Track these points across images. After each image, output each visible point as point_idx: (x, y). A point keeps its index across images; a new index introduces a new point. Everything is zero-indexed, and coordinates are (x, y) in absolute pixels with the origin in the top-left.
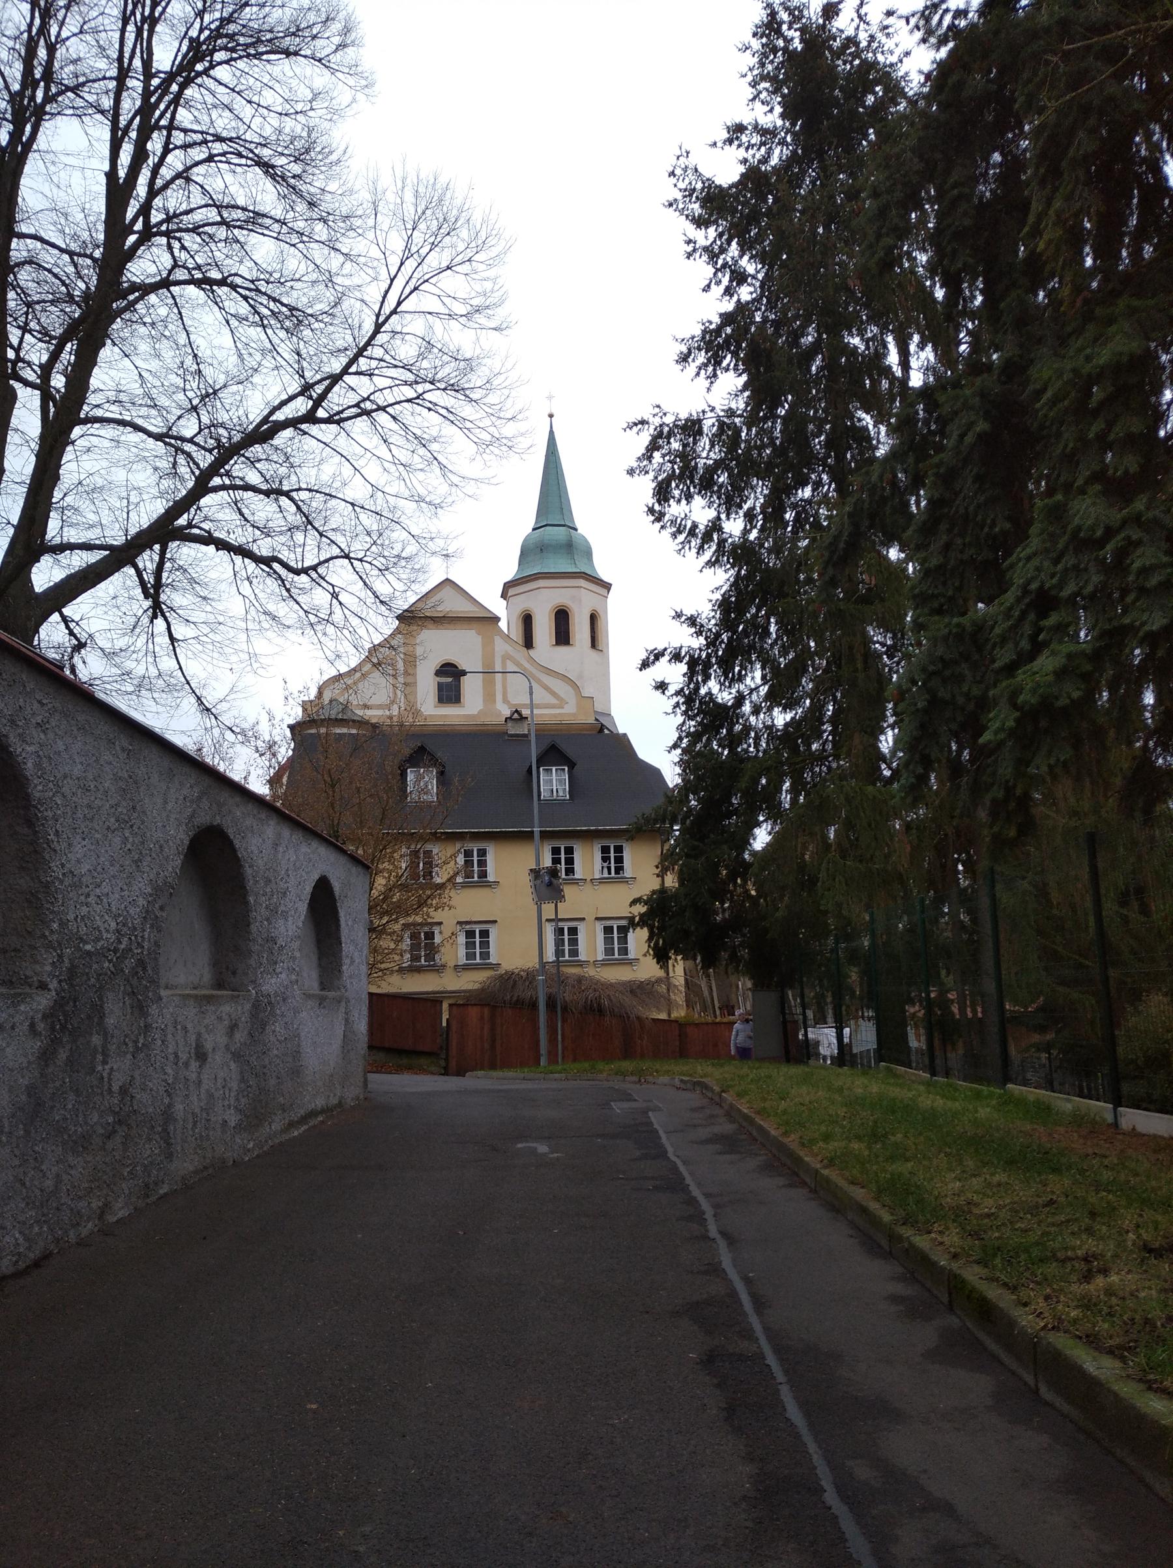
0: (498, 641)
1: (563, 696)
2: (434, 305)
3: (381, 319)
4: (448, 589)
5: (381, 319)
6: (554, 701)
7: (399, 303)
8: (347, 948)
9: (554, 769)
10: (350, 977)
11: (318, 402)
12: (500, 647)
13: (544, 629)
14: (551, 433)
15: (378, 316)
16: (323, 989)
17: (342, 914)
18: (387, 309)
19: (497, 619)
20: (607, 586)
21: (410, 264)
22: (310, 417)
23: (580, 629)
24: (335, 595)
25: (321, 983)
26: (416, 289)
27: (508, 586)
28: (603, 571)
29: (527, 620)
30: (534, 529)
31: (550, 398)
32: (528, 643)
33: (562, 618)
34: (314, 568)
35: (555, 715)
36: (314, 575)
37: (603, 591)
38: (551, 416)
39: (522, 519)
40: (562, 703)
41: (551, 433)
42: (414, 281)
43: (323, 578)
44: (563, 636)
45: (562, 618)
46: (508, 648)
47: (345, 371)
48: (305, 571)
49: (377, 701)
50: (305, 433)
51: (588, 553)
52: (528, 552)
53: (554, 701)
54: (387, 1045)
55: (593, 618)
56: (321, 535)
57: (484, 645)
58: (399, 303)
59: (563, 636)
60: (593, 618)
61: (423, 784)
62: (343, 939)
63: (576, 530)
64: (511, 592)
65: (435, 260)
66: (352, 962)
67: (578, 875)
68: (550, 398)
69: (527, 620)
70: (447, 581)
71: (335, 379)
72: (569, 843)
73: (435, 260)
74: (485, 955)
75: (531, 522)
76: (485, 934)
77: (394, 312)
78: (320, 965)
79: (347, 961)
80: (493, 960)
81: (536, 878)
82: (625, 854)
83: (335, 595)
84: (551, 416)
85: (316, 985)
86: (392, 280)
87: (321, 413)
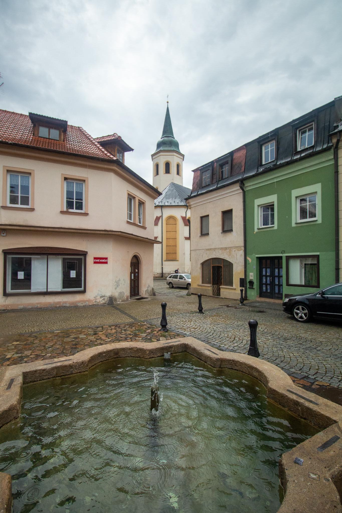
13: (162, 168)
14: (168, 108)
33: (167, 165)
39: (158, 136)
41: (168, 108)
44: (168, 171)
45: (167, 165)
52: (159, 145)
59: (168, 171)
84: (168, 102)
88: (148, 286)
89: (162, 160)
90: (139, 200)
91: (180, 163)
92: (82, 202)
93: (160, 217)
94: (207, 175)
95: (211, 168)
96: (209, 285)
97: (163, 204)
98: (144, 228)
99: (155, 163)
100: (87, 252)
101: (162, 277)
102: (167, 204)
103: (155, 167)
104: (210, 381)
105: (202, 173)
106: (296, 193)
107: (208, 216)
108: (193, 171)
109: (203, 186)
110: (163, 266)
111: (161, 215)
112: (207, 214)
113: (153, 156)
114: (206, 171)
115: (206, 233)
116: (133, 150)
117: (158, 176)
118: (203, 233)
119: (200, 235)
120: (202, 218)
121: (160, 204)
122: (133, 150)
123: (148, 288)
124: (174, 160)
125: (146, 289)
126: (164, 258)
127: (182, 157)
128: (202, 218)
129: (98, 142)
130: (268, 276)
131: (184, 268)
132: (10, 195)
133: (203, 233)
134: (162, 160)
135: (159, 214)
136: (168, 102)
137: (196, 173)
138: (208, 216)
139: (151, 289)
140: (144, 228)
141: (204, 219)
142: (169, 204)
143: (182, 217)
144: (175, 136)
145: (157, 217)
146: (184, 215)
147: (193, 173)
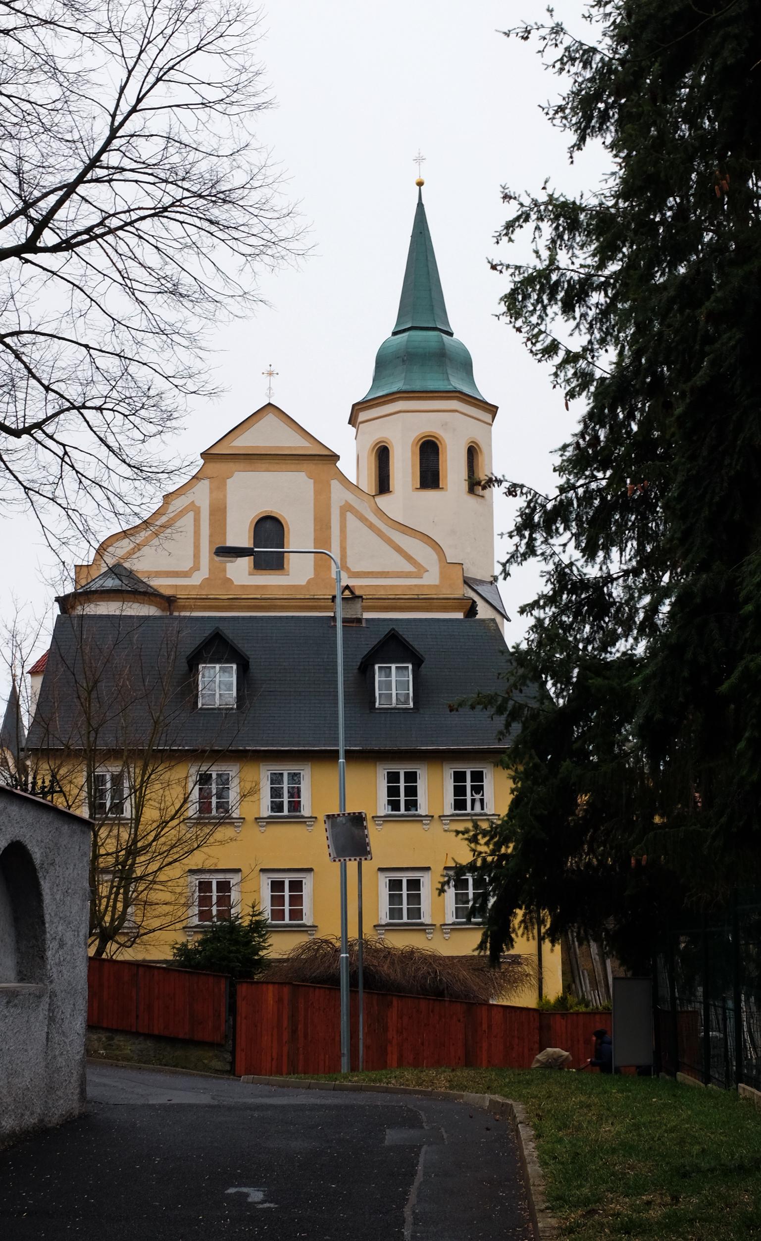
0: (335, 485)
1: (420, 560)
2: (185, 95)
3: (119, 119)
4: (270, 418)
5: (119, 119)
6: (409, 568)
7: (139, 100)
8: (53, 927)
9: (393, 666)
10: (59, 964)
11: (40, 226)
12: (338, 495)
13: (404, 467)
14: (420, 206)
15: (113, 116)
16: (21, 980)
17: (46, 886)
18: (125, 108)
19: (335, 457)
20: (493, 410)
21: (152, 50)
22: (31, 246)
23: (454, 467)
24: (64, 458)
25: (20, 973)
26: (159, 80)
27: (357, 408)
28: (486, 390)
29: (383, 454)
30: (395, 334)
31: (419, 160)
32: (383, 485)
33: (429, 451)
34: (38, 425)
35: (410, 587)
36: (39, 435)
37: (487, 417)
38: (420, 184)
39: (379, 317)
40: (421, 570)
41: (420, 206)
42: (155, 71)
43: (51, 437)
44: (430, 477)
45: (429, 451)
46: (350, 498)
47: (80, 180)
48: (27, 431)
49: (176, 564)
50: (27, 261)
51: (465, 365)
52: (385, 363)
53: (409, 568)
54: (156, 1032)
55: (472, 453)
56: (47, 389)
57: (317, 493)
58: (139, 100)
59: (430, 477)
60: (472, 453)
61: (218, 684)
62: (47, 918)
63: (451, 334)
64: (362, 416)
65: (182, 42)
66: (62, 945)
67: (422, 810)
68: (419, 160)
69: (383, 454)
70: (269, 404)
71: (70, 189)
72: (410, 768)
73: (182, 42)
74: (296, 914)
75: (391, 323)
76: (296, 886)
77: (134, 110)
78: (18, 950)
79: (54, 945)
80: (307, 920)
81: (333, 826)
82: (486, 783)
83: (64, 458)
84: (420, 184)
85: (12, 974)
86: (130, 72)
87: (48, 238)
89: (402, 430)
92: (272, 797)
100: (497, 408)
106: (410, 666)
124: (453, 429)
126: (205, 877)
129: (415, 1149)
130: (105, 871)
132: (272, 788)
134: (402, 430)
144: (454, 326)
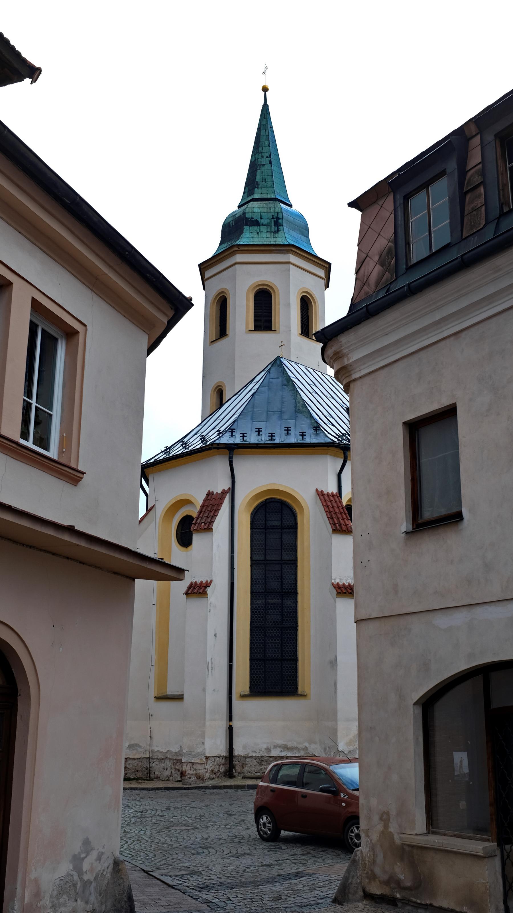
13: (241, 312)
33: (264, 303)
39: (229, 198)
59: (264, 318)
84: (265, 89)
88: (77, 847)
90: (35, 303)
91: (315, 292)
93: (224, 493)
94: (433, 214)
95: (452, 166)
96: (477, 847)
97: (238, 440)
98: (72, 475)
99: (214, 293)
101: (229, 774)
102: (253, 439)
103: (215, 310)
104: (347, 350)
105: (407, 198)
107: (449, 413)
108: (351, 205)
109: (415, 258)
110: (235, 724)
111: (226, 485)
112: (445, 402)
113: (203, 267)
114: (426, 185)
115: (443, 511)
116: (33, 72)
117: (224, 342)
118: (428, 513)
119: (404, 525)
120: (414, 428)
121: (226, 439)
122: (33, 72)
123: (77, 861)
125: (65, 868)
127: (322, 273)
128: (414, 428)
131: (334, 732)
133: (428, 513)
135: (221, 484)
136: (265, 89)
137: (374, 210)
138: (449, 413)
139: (107, 863)
140: (72, 475)
141: (428, 437)
142: (264, 439)
143: (321, 494)
145: (210, 494)
146: (332, 488)
147: (357, 214)
